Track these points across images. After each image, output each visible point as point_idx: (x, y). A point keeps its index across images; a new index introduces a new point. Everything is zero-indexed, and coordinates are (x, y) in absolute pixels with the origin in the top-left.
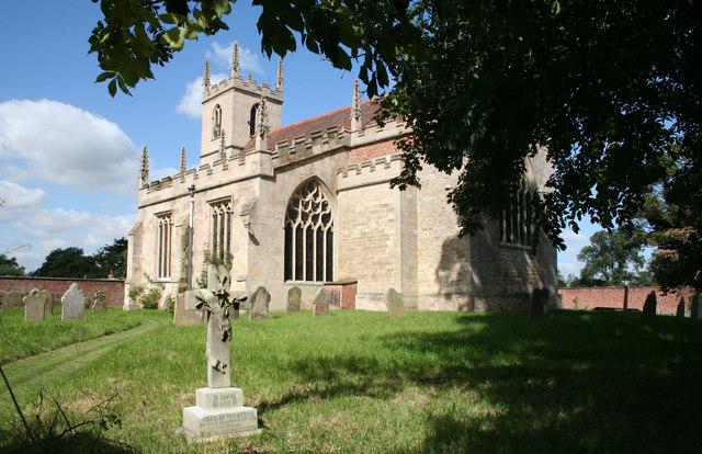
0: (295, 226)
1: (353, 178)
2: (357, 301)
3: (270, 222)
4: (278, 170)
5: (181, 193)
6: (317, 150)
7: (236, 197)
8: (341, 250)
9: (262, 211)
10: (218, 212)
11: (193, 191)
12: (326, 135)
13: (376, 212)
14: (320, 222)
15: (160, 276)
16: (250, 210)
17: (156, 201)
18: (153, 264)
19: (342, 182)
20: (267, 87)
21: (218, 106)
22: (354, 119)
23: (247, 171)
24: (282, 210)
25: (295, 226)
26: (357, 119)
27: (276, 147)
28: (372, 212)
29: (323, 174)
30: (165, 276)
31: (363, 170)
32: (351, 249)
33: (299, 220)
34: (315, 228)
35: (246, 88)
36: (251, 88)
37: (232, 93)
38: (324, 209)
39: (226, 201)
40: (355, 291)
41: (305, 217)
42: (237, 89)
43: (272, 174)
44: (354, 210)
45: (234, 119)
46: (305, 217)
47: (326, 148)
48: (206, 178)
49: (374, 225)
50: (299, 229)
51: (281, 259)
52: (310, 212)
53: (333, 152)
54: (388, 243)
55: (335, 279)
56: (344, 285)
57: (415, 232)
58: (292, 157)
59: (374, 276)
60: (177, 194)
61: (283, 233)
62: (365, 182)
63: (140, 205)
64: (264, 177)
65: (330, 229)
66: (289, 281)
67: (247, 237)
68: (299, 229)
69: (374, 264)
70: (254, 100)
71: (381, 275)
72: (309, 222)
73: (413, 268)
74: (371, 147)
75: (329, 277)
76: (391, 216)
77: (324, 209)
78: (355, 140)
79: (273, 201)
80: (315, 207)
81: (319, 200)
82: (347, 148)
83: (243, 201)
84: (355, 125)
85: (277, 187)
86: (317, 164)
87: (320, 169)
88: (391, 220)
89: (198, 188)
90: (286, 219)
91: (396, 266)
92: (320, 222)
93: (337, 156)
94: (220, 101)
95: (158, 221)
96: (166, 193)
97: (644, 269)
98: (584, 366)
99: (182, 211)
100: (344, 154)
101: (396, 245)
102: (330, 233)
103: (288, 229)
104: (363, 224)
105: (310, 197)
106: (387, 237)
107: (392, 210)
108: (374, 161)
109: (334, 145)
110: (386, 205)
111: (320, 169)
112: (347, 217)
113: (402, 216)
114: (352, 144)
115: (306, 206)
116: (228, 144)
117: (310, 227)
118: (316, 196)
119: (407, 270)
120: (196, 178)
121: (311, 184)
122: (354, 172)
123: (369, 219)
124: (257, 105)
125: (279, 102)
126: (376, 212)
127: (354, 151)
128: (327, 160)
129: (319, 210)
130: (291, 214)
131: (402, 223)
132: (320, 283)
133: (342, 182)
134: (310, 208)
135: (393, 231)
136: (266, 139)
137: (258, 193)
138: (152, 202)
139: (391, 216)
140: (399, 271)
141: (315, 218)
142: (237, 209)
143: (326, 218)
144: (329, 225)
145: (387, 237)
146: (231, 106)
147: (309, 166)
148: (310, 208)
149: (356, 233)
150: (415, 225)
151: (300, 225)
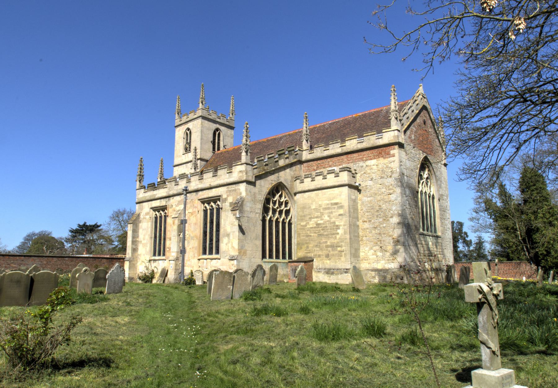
0: (268, 218)
1: (308, 184)
2: (314, 274)
3: (252, 215)
4: (259, 177)
5: (175, 192)
6: (282, 163)
7: (224, 196)
8: (299, 235)
9: (247, 207)
10: (208, 207)
11: (186, 191)
12: (287, 152)
13: (328, 208)
14: (283, 216)
15: (154, 255)
16: (238, 206)
17: (152, 198)
18: (149, 245)
19: (299, 187)
20: (224, 116)
21: (188, 129)
22: (305, 141)
23: (235, 177)
24: (259, 207)
25: (268, 218)
26: (307, 141)
27: (256, 161)
28: (325, 209)
29: (286, 180)
30: (159, 255)
31: (305, 180)
32: (308, 236)
33: (270, 213)
34: (281, 220)
35: (210, 117)
36: (213, 117)
37: (200, 120)
38: (286, 206)
39: (216, 199)
40: (312, 267)
41: (274, 211)
42: (204, 118)
43: (253, 180)
44: (310, 207)
45: (201, 139)
46: (274, 211)
47: (287, 162)
48: (198, 182)
49: (326, 218)
50: (271, 221)
51: (259, 243)
52: (277, 208)
53: (291, 165)
54: (339, 231)
55: (294, 258)
56: (305, 262)
57: (358, 223)
58: (266, 168)
59: (327, 256)
60: (171, 193)
61: (261, 223)
62: (319, 186)
63: (137, 201)
64: (249, 182)
65: (290, 221)
66: (264, 260)
67: (236, 228)
68: (271, 221)
69: (327, 246)
70: (215, 126)
71: (333, 255)
72: (277, 215)
73: (357, 250)
74: (319, 162)
75: (290, 257)
76: (341, 211)
77: (286, 206)
78: (306, 156)
79: (254, 200)
80: (281, 204)
81: (283, 199)
82: (300, 162)
83: (230, 200)
84: (305, 145)
85: (257, 189)
86: (282, 174)
87: (285, 176)
88: (340, 215)
89: (191, 188)
90: (263, 213)
91: (345, 248)
92: (283, 216)
93: (294, 168)
94: (190, 125)
95: (153, 214)
96: (161, 192)
97: (471, 248)
98: (126, 319)
99: (175, 205)
100: (298, 166)
101: (345, 233)
102: (290, 224)
103: (264, 220)
104: (317, 217)
105: (277, 197)
106: (338, 227)
107: (341, 207)
108: (314, 173)
109: (292, 160)
110: (336, 204)
111: (285, 176)
112: (303, 212)
113: (349, 212)
114: (304, 158)
115: (274, 203)
116: (198, 157)
117: (277, 219)
118: (281, 196)
119: (353, 251)
120: (189, 181)
121: (278, 188)
122: (310, 179)
123: (322, 214)
124: (217, 130)
125: (232, 128)
126: (328, 208)
127: (305, 164)
128: (288, 170)
129: (283, 207)
130: (266, 210)
131: (350, 216)
132: (271, 260)
133: (299, 187)
134: (277, 205)
135: (343, 223)
136: (249, 154)
137: (244, 194)
138: (148, 198)
139: (341, 211)
140: (348, 252)
141: (281, 213)
142: (226, 206)
143: (288, 212)
144: (289, 218)
145: (338, 227)
146: (199, 129)
147: (277, 174)
148: (277, 205)
149: (312, 224)
150: (357, 219)
151: (271, 218)
